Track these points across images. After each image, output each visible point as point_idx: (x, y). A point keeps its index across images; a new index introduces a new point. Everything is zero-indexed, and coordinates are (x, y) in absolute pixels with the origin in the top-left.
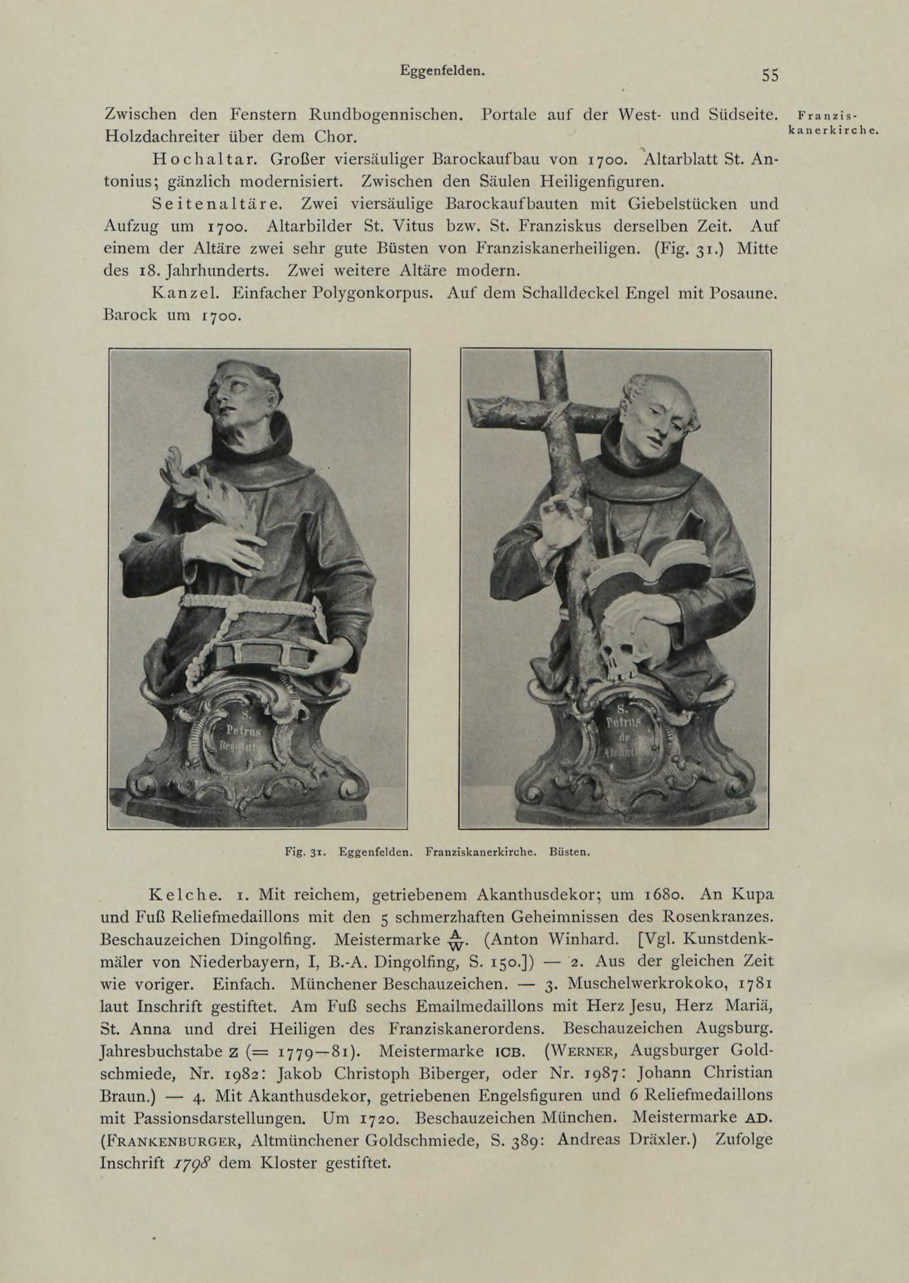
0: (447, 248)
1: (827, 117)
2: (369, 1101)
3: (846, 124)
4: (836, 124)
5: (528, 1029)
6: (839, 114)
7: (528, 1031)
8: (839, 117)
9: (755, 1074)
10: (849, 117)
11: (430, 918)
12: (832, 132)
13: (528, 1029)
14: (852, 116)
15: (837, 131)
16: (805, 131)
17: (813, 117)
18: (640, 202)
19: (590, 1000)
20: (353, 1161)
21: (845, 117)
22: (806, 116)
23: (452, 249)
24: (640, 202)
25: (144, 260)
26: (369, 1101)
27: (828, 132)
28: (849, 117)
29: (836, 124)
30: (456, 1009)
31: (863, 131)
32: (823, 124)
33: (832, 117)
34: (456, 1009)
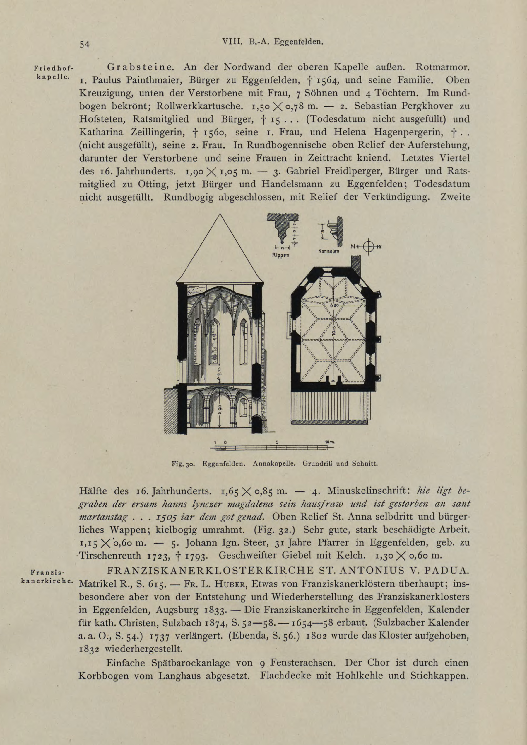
0: (159, 597)
1: (47, 573)
2: (381, 174)
3: (54, 577)
4: (48, 577)
5: (284, 663)
6: (54, 571)
7: (284, 664)
8: (54, 573)
9: (386, 107)
10: (60, 573)
11: (455, 68)
12: (46, 582)
13: (284, 663)
14: (61, 573)
15: (49, 581)
16: (30, 581)
17: (39, 573)
18: (289, 554)
19: (303, 573)
20: (381, 105)
21: (57, 573)
22: (35, 573)
23: (162, 598)
24: (289, 554)
25: (443, 510)
26: (381, 174)
27: (44, 582)
28: (60, 573)
29: (48, 577)
30: (420, 81)
31: (64, 581)
32: (41, 577)
33: (50, 573)
34: (420, 81)
